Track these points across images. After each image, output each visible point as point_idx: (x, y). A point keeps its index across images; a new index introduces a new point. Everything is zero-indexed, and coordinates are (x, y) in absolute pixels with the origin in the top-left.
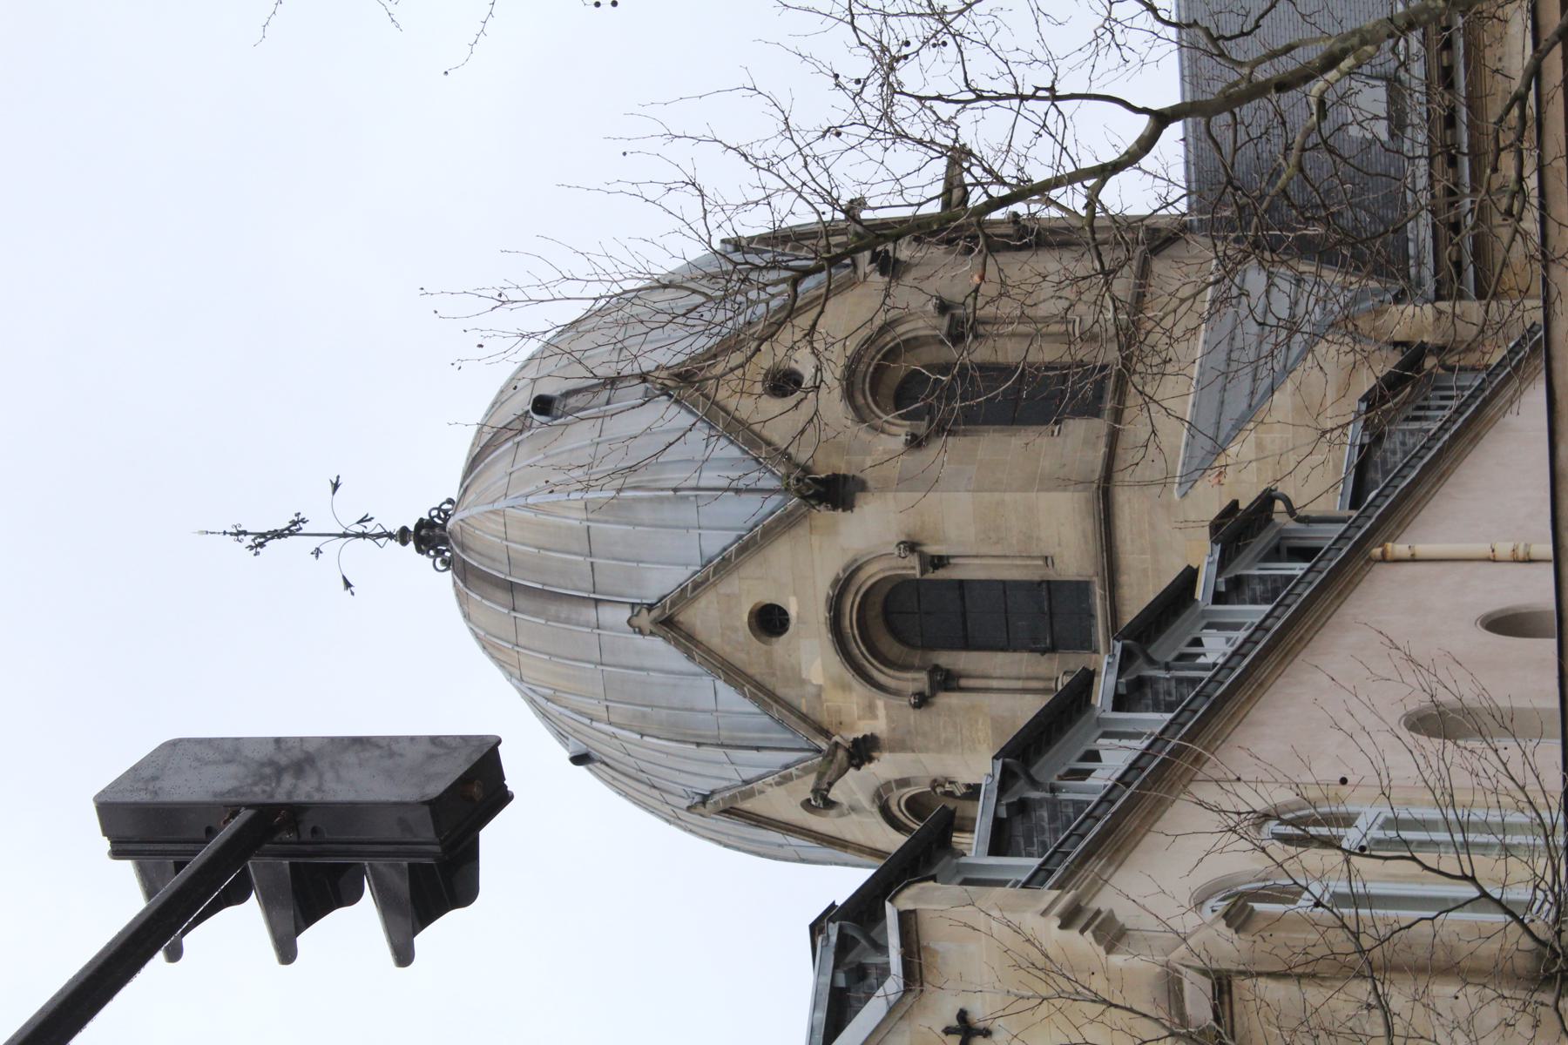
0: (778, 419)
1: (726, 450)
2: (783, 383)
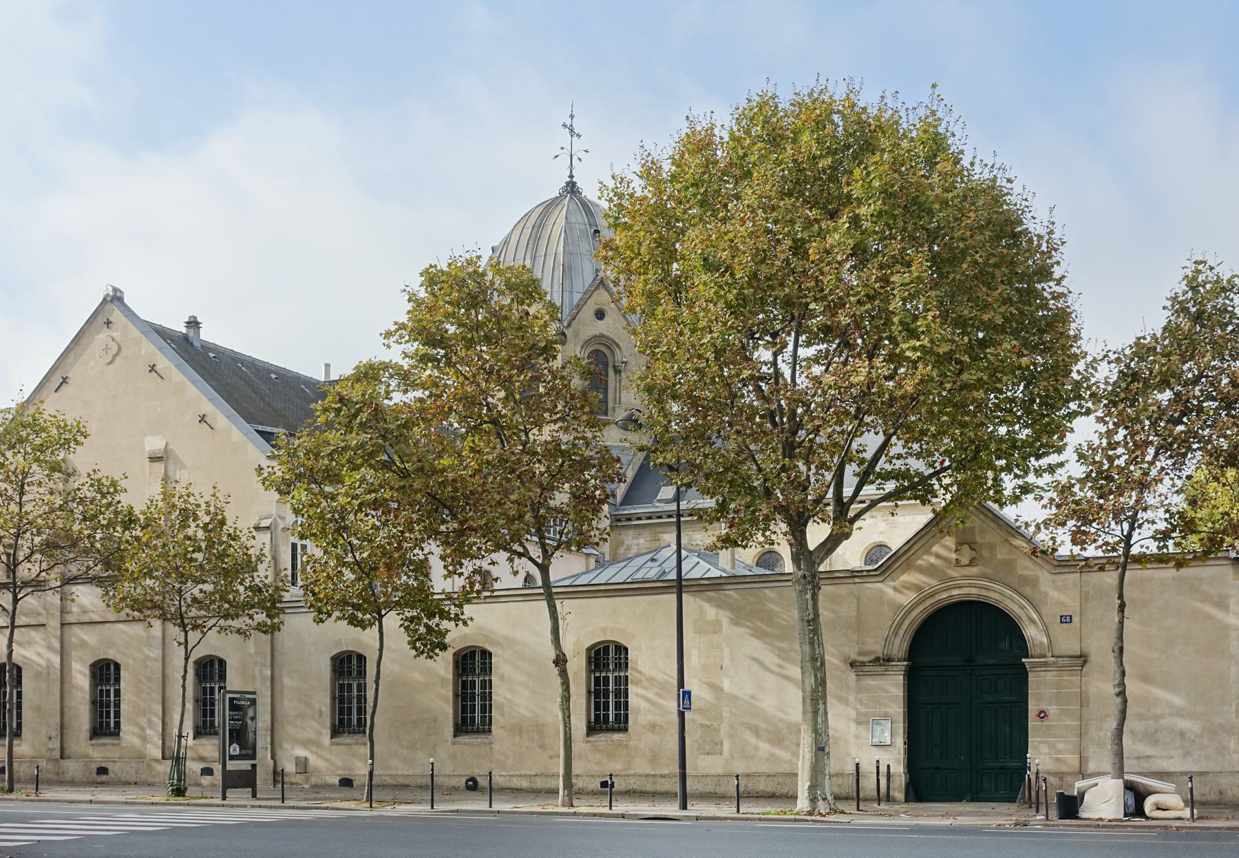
0: (588, 312)
1: (577, 297)
2: (600, 315)
